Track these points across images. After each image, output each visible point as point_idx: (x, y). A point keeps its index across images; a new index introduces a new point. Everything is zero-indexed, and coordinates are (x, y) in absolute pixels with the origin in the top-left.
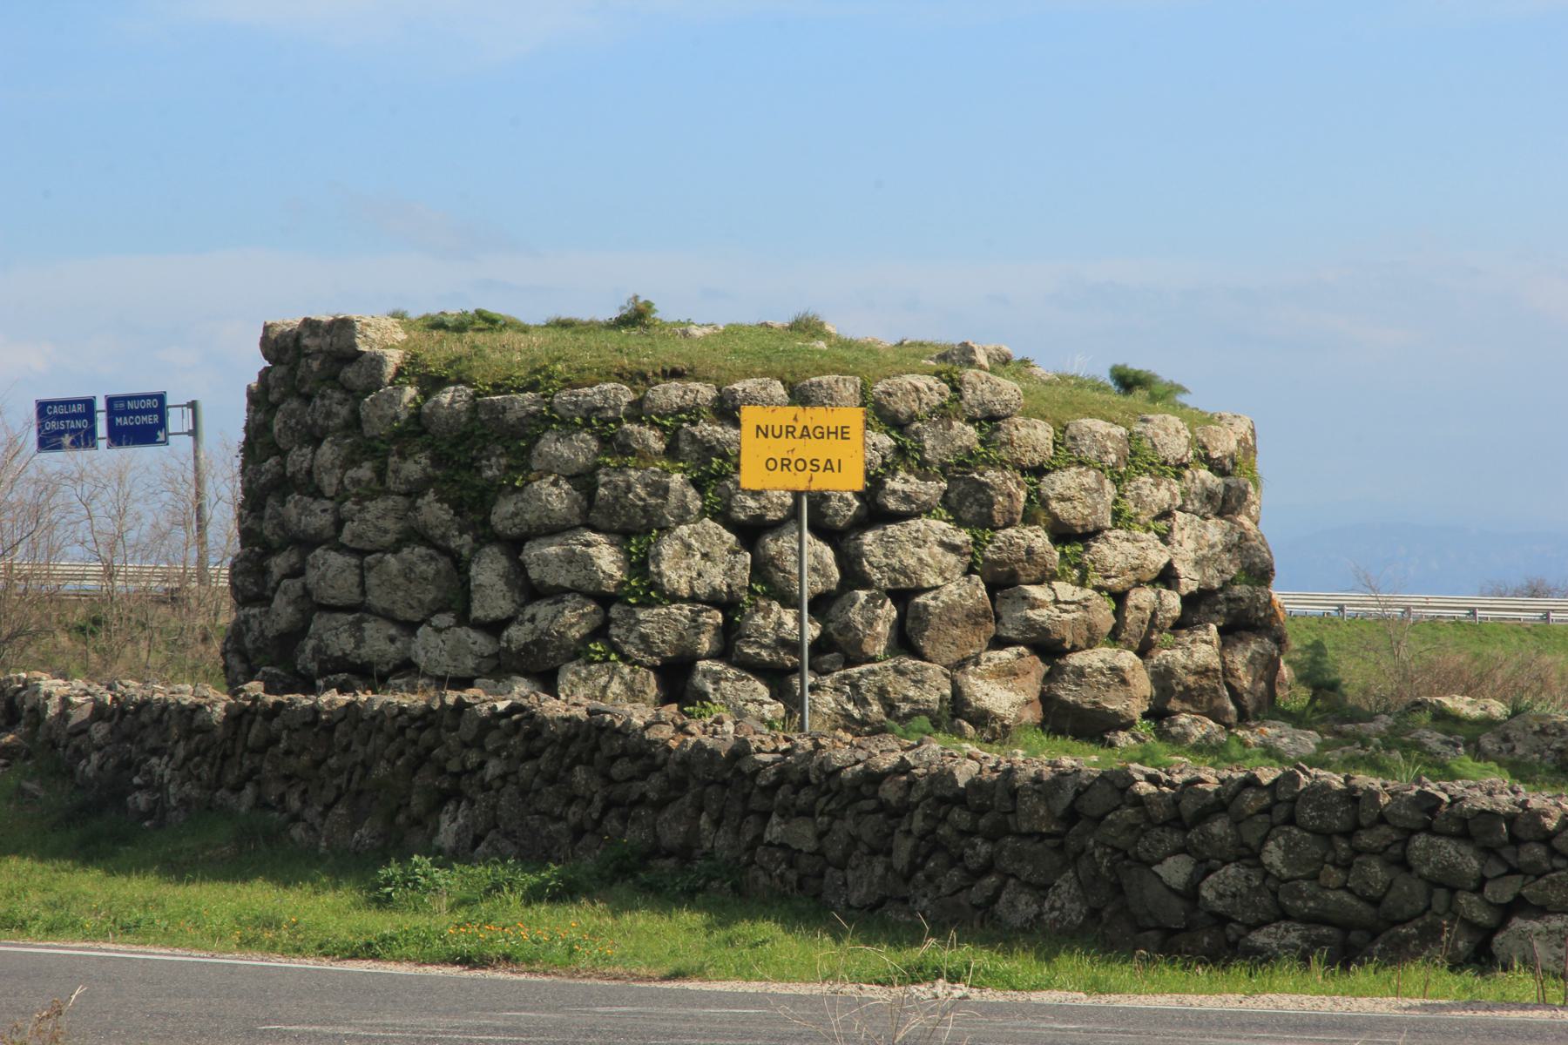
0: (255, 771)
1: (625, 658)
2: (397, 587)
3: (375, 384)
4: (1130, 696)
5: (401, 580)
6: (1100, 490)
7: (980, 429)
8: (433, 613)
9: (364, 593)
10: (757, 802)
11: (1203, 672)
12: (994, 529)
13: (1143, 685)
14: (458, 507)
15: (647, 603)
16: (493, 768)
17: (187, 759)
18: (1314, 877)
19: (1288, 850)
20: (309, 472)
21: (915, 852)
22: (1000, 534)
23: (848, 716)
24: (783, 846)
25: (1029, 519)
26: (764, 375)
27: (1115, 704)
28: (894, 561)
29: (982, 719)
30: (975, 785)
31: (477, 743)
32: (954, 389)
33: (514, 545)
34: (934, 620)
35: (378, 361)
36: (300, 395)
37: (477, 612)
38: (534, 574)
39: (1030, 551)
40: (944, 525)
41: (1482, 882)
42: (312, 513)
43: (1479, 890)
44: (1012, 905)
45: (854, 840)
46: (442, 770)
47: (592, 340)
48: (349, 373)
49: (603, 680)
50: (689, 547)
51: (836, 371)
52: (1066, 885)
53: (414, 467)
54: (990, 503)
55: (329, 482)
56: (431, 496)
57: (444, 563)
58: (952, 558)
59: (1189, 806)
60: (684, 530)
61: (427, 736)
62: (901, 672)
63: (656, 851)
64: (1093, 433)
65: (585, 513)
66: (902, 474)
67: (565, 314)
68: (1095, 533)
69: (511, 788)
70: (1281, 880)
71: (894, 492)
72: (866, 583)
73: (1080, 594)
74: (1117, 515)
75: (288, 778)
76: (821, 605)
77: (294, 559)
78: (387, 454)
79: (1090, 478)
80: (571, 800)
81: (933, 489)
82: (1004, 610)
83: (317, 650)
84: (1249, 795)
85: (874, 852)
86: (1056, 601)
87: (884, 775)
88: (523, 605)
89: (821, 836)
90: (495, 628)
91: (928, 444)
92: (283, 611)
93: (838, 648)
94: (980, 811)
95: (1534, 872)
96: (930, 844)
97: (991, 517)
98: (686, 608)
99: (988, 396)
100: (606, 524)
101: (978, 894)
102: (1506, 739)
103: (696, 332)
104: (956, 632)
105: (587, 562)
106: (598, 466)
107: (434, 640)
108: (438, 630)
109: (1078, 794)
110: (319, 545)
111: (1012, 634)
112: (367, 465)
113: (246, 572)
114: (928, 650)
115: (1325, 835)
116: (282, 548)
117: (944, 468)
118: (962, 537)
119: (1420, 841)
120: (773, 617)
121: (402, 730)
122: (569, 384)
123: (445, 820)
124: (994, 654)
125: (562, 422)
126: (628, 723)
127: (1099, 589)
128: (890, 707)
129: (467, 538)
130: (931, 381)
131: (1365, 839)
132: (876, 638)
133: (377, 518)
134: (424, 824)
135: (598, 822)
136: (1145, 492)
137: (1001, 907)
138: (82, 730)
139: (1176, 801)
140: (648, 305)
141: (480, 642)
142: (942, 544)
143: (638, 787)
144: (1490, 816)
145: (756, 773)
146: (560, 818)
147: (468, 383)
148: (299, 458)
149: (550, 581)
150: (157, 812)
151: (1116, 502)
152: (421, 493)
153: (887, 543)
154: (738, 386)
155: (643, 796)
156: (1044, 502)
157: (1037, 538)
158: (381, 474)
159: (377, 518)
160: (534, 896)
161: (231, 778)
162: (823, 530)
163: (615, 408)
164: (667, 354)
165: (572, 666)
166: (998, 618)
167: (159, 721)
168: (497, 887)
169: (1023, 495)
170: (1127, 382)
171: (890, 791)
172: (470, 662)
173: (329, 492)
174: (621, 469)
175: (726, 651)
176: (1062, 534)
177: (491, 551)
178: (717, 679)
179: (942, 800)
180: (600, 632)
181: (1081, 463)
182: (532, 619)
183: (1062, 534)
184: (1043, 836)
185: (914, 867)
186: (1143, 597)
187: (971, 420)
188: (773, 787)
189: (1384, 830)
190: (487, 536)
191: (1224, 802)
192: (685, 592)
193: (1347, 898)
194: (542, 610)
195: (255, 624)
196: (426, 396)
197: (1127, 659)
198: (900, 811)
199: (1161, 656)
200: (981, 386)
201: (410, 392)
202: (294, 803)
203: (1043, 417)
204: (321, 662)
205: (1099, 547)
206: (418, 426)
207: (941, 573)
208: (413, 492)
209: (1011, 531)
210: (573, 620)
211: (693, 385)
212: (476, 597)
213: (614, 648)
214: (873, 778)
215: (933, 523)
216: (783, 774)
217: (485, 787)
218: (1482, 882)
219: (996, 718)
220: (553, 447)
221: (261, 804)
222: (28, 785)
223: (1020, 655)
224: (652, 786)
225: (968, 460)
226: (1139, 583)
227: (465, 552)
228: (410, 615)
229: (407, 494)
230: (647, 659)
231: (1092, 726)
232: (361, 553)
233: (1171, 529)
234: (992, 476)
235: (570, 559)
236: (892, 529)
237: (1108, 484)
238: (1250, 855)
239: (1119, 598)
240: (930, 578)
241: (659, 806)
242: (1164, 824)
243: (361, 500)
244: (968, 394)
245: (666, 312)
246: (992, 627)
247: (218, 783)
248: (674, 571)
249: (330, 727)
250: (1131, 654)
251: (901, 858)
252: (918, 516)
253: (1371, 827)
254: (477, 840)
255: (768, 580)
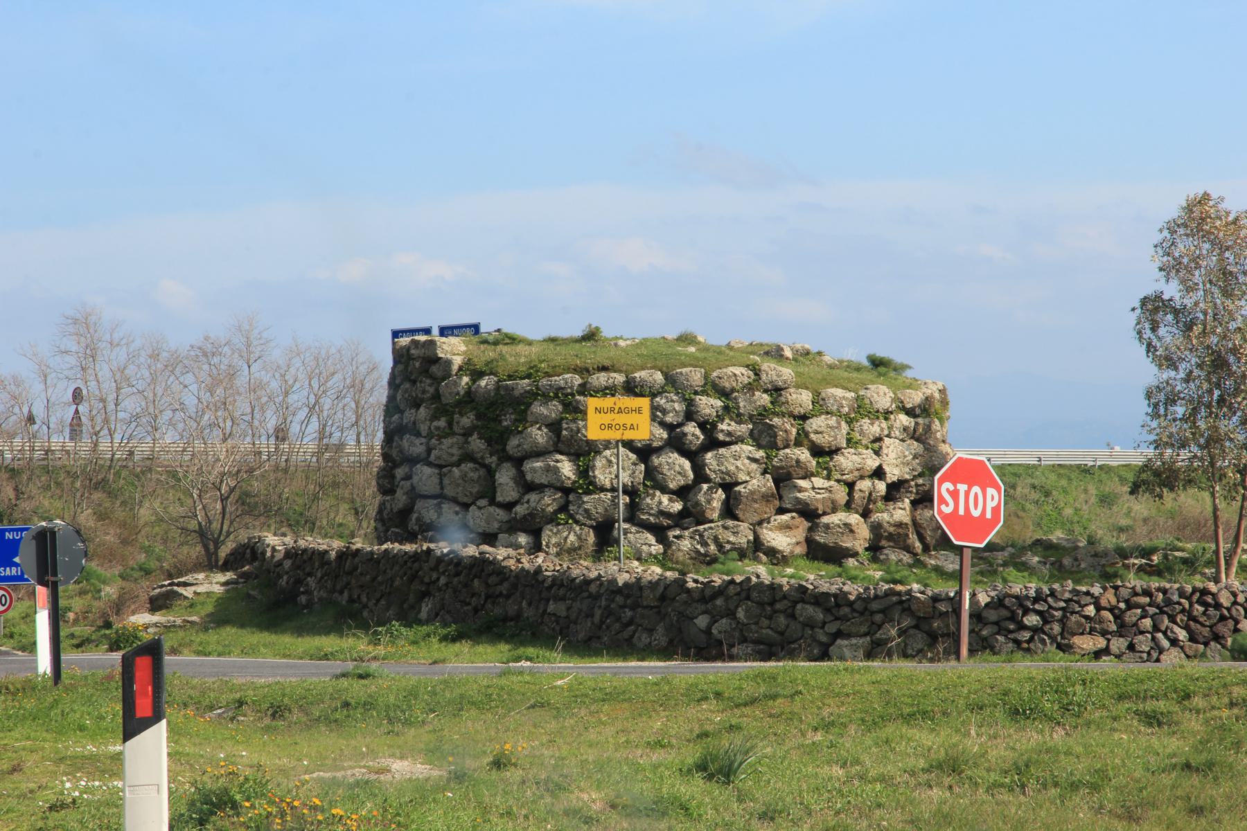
0: (348, 584)
1: (577, 522)
2: (458, 485)
3: (447, 375)
4: (855, 539)
5: (460, 481)
6: (839, 427)
7: (771, 395)
8: (477, 499)
9: (442, 488)
10: (544, 594)
11: (900, 525)
12: (779, 449)
13: (864, 532)
14: (489, 442)
15: (588, 492)
16: (443, 580)
17: (322, 578)
18: (756, 623)
19: (747, 611)
20: (414, 423)
21: (602, 616)
22: (781, 452)
23: (698, 552)
24: (554, 615)
25: (798, 444)
26: (652, 368)
27: (847, 543)
28: (723, 468)
29: (772, 553)
30: (626, 584)
31: (435, 568)
32: (756, 374)
33: (518, 462)
34: (744, 500)
35: (449, 363)
36: (410, 380)
37: (499, 498)
38: (529, 477)
39: (798, 461)
40: (751, 448)
41: (824, 623)
42: (415, 445)
43: (823, 627)
44: (640, 638)
45: (581, 610)
46: (422, 582)
47: (563, 350)
48: (434, 369)
49: (565, 534)
50: (610, 462)
51: (691, 365)
52: (660, 629)
53: (467, 420)
54: (775, 436)
55: (424, 429)
56: (475, 436)
57: (482, 472)
58: (754, 466)
59: (708, 593)
60: (608, 453)
61: (416, 565)
62: (726, 528)
63: (505, 619)
64: (835, 397)
65: (556, 444)
66: (727, 421)
67: (553, 335)
68: (837, 451)
69: (450, 590)
70: (743, 624)
71: (722, 431)
72: (707, 480)
73: (827, 484)
74: (849, 441)
75: (362, 586)
76: (682, 493)
77: (407, 470)
78: (453, 413)
79: (833, 421)
80: (473, 595)
81: (744, 429)
82: (784, 493)
83: (418, 519)
84: (731, 587)
85: (587, 616)
86: (814, 488)
87: (592, 581)
88: (524, 494)
89: (568, 609)
90: (509, 506)
91: (741, 404)
92: (401, 498)
93: (692, 516)
94: (628, 596)
95: (844, 619)
96: (608, 612)
97: (776, 443)
98: (609, 495)
99: (775, 378)
100: (567, 450)
101: (626, 634)
102: (1076, 560)
103: (622, 343)
104: (756, 506)
105: (556, 470)
106: (562, 419)
107: (477, 513)
108: (480, 508)
109: (665, 588)
110: (418, 462)
111: (789, 506)
112: (443, 419)
113: (384, 477)
114: (741, 516)
115: (761, 604)
116: (401, 464)
117: (751, 417)
118: (760, 454)
119: (799, 606)
120: (657, 499)
121: (406, 562)
122: (548, 375)
123: (424, 605)
124: (778, 517)
125: (544, 395)
126: (495, 558)
127: (838, 481)
128: (720, 547)
129: (494, 458)
130: (743, 370)
131: (778, 606)
132: (713, 509)
133: (448, 448)
134: (416, 607)
135: (483, 605)
136: (865, 427)
137: (635, 640)
138: (280, 564)
139: (703, 590)
140: (597, 329)
141: (501, 514)
142: (749, 458)
143: (499, 588)
144: (827, 595)
145: (544, 581)
146: (469, 604)
147: (495, 375)
148: (409, 415)
149: (537, 481)
150: (309, 605)
151: (848, 434)
152: (471, 435)
153: (719, 458)
154: (637, 375)
155: (501, 593)
156: (807, 434)
157: (804, 455)
158: (450, 424)
159: (448, 448)
160: (444, 639)
161: (338, 587)
162: (685, 453)
163: (572, 388)
164: (602, 357)
165: (549, 526)
166: (781, 498)
167: (311, 559)
168: (428, 635)
169: (794, 431)
170: (877, 363)
171: (593, 588)
172: (496, 525)
173: (424, 434)
174: (574, 420)
175: (631, 518)
176: (817, 451)
177: (507, 465)
178: (626, 532)
179: (613, 592)
180: (564, 508)
181: (828, 413)
182: (528, 502)
183: (817, 451)
184: (652, 608)
185: (602, 622)
186: (864, 485)
187: (766, 391)
188: (551, 587)
189: (786, 602)
190: (505, 457)
191: (721, 591)
192: (608, 486)
193: (770, 632)
194: (533, 497)
195: (388, 506)
196: (474, 381)
197: (854, 519)
198: (596, 597)
199: (877, 517)
200: (774, 371)
201: (466, 379)
202: (364, 599)
203: (807, 388)
204: (420, 526)
205: (839, 459)
206: (470, 397)
207: (749, 474)
208: (467, 434)
209: (787, 451)
210: (549, 502)
211: (613, 375)
212: (498, 490)
213: (571, 517)
214: (587, 582)
215: (744, 447)
216: (554, 578)
217: (440, 590)
218: (824, 623)
219: (778, 552)
220: (539, 409)
221: (351, 600)
222: (252, 593)
223: (793, 518)
224: (504, 589)
225: (764, 413)
226: (862, 478)
227: (493, 466)
228: (465, 500)
229: (464, 435)
230: (589, 522)
231: (824, 553)
232: (440, 467)
233: (881, 447)
234: (776, 421)
235: (548, 469)
236: (722, 451)
237: (843, 424)
238: (731, 614)
239: (851, 486)
240: (742, 477)
241: (508, 597)
242: (698, 601)
243: (440, 438)
244: (764, 377)
245: (607, 332)
246: (777, 503)
247: (333, 591)
248: (602, 476)
249: (378, 562)
250: (857, 516)
251: (597, 619)
252: (736, 443)
253: (780, 600)
254: (437, 615)
255: (654, 479)
